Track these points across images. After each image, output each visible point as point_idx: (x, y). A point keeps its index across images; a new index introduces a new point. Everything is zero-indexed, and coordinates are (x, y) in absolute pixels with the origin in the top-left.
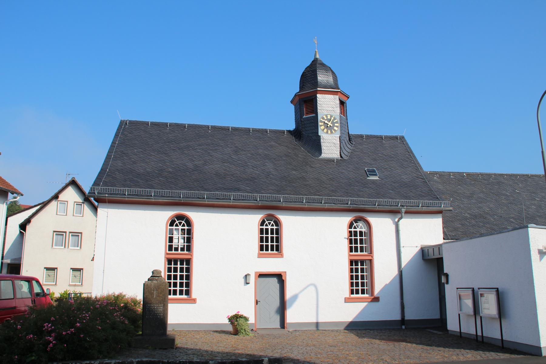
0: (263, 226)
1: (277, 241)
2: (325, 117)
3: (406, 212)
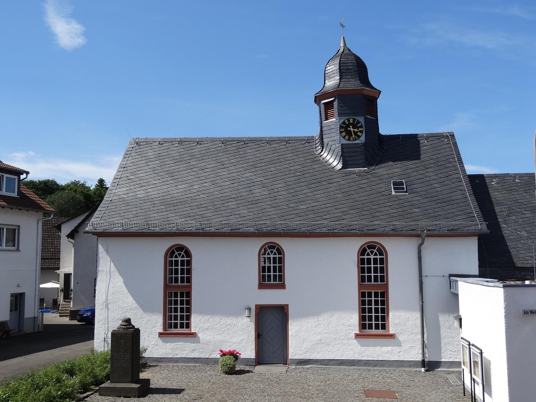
0: (364, 256)
1: (280, 271)
3: (428, 236)
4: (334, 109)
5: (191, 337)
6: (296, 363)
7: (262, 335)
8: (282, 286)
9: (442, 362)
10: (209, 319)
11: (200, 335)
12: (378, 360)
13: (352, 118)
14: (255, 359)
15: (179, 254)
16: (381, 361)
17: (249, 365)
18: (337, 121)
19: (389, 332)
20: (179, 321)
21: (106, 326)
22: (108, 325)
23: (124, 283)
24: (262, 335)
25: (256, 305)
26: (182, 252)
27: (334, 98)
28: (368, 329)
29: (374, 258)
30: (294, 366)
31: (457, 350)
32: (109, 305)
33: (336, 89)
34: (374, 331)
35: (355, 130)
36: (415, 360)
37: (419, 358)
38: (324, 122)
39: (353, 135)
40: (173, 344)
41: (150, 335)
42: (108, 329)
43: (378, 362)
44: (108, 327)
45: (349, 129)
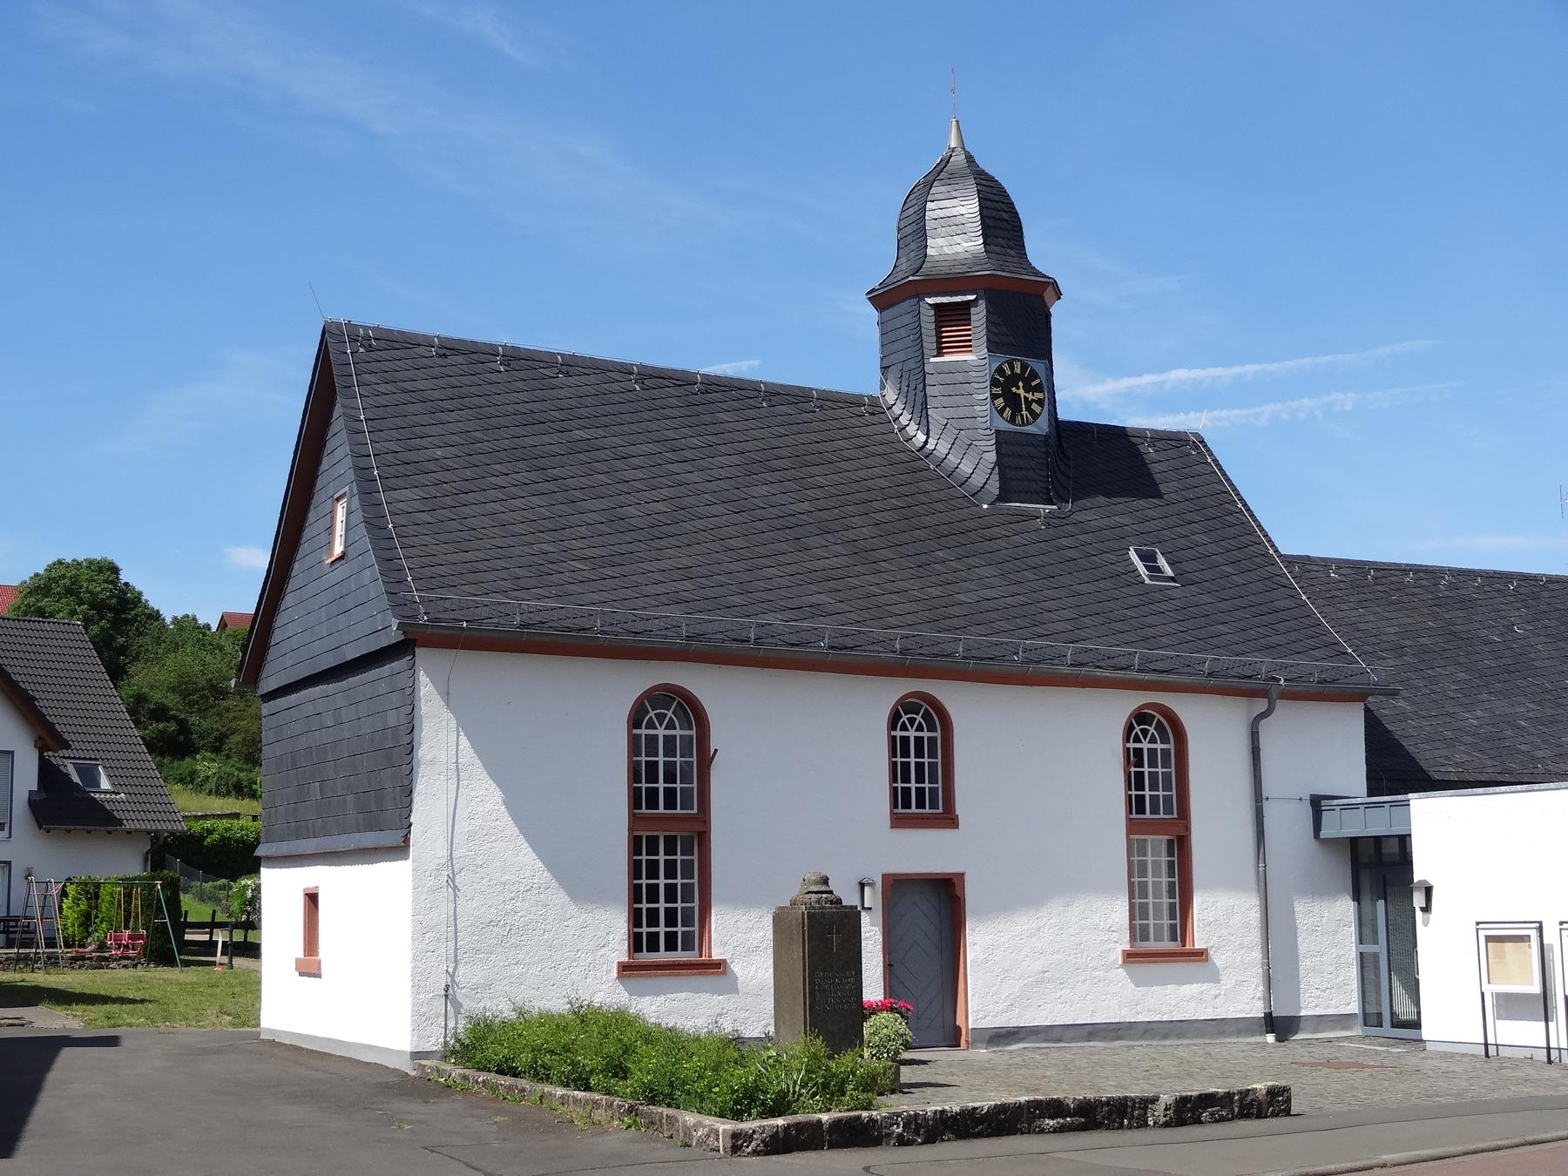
2: (1006, 367)
4: (970, 325)
5: (713, 973)
6: (987, 1038)
8: (948, 819)
9: (1302, 1019)
10: (762, 919)
11: (736, 968)
12: (1171, 1021)
13: (1019, 360)
15: (661, 717)
16: (1180, 1024)
18: (983, 362)
19: (1194, 946)
20: (662, 929)
21: (451, 944)
22: (456, 943)
23: (505, 803)
25: (884, 876)
26: (918, 715)
27: (975, 296)
28: (647, 951)
29: (665, 737)
31: (1329, 986)
32: (457, 877)
33: (989, 272)
34: (663, 956)
35: (1027, 395)
36: (1248, 1016)
37: (1257, 1010)
38: (932, 360)
39: (1024, 409)
40: (661, 999)
41: (589, 971)
42: (456, 956)
43: (1172, 1025)
44: (456, 949)
45: (1014, 389)
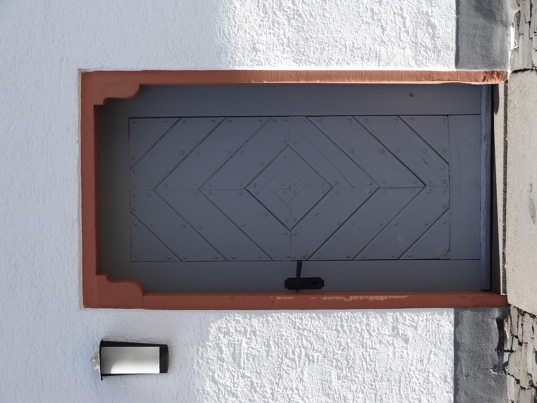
6: (481, 21)
7: (300, 263)
14: (458, 308)
17: (500, 349)
24: (300, 263)
30: (504, 40)
